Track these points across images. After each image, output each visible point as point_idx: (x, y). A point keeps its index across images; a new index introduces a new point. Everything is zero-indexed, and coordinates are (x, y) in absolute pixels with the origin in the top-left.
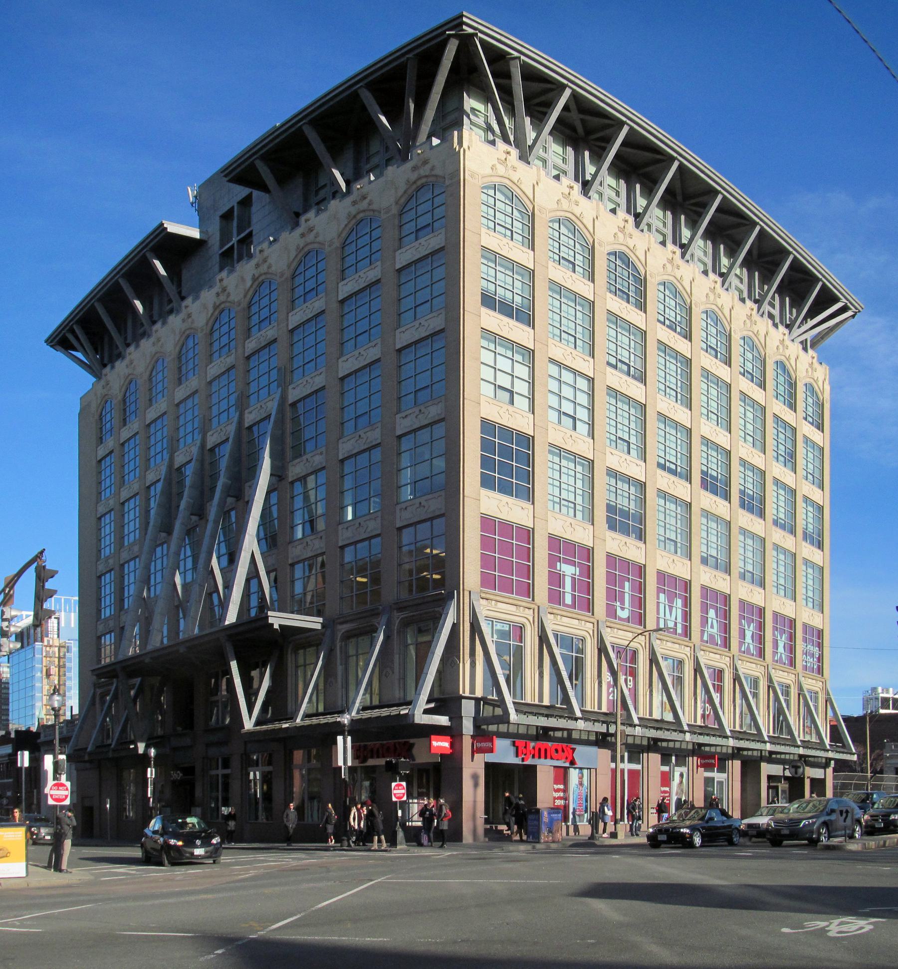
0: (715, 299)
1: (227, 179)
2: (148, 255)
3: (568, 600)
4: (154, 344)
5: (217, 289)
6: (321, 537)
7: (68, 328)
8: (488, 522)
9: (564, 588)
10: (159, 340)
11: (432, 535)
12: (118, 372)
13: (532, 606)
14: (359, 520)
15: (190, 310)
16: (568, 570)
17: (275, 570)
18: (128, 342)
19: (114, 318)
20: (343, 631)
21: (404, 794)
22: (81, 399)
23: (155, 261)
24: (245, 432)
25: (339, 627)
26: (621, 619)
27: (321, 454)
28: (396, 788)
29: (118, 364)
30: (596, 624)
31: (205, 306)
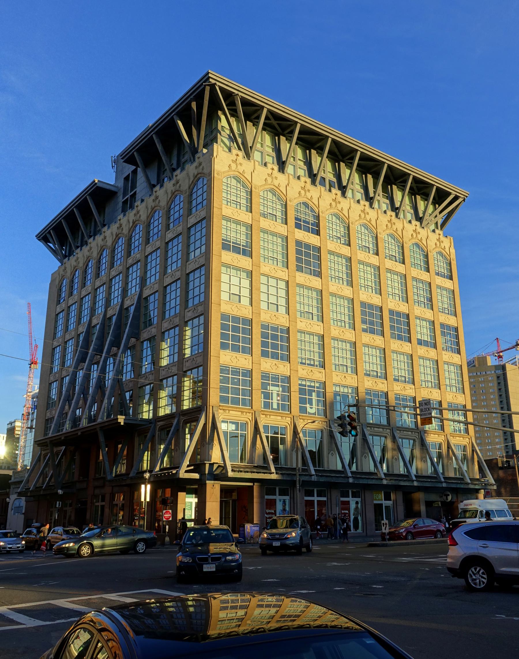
0: (392, 226)
1: (123, 160)
2: (175, 117)
3: (275, 406)
4: (174, 185)
5: (117, 225)
6: (153, 374)
7: (48, 231)
8: (224, 370)
9: (272, 400)
10: (177, 182)
11: (173, 383)
12: (81, 254)
13: (251, 411)
14: (194, 357)
15: (201, 159)
16: (274, 390)
17: (132, 390)
18: (173, 167)
19: (84, 219)
20: (159, 426)
21: (170, 517)
22: (52, 275)
23: (178, 121)
24: (143, 301)
25: (158, 423)
26: (310, 413)
27: (155, 327)
28: (166, 513)
29: (84, 248)
30: (292, 418)
31: (166, 192)
